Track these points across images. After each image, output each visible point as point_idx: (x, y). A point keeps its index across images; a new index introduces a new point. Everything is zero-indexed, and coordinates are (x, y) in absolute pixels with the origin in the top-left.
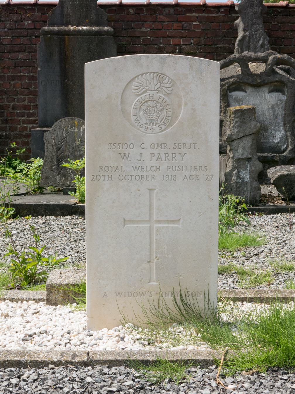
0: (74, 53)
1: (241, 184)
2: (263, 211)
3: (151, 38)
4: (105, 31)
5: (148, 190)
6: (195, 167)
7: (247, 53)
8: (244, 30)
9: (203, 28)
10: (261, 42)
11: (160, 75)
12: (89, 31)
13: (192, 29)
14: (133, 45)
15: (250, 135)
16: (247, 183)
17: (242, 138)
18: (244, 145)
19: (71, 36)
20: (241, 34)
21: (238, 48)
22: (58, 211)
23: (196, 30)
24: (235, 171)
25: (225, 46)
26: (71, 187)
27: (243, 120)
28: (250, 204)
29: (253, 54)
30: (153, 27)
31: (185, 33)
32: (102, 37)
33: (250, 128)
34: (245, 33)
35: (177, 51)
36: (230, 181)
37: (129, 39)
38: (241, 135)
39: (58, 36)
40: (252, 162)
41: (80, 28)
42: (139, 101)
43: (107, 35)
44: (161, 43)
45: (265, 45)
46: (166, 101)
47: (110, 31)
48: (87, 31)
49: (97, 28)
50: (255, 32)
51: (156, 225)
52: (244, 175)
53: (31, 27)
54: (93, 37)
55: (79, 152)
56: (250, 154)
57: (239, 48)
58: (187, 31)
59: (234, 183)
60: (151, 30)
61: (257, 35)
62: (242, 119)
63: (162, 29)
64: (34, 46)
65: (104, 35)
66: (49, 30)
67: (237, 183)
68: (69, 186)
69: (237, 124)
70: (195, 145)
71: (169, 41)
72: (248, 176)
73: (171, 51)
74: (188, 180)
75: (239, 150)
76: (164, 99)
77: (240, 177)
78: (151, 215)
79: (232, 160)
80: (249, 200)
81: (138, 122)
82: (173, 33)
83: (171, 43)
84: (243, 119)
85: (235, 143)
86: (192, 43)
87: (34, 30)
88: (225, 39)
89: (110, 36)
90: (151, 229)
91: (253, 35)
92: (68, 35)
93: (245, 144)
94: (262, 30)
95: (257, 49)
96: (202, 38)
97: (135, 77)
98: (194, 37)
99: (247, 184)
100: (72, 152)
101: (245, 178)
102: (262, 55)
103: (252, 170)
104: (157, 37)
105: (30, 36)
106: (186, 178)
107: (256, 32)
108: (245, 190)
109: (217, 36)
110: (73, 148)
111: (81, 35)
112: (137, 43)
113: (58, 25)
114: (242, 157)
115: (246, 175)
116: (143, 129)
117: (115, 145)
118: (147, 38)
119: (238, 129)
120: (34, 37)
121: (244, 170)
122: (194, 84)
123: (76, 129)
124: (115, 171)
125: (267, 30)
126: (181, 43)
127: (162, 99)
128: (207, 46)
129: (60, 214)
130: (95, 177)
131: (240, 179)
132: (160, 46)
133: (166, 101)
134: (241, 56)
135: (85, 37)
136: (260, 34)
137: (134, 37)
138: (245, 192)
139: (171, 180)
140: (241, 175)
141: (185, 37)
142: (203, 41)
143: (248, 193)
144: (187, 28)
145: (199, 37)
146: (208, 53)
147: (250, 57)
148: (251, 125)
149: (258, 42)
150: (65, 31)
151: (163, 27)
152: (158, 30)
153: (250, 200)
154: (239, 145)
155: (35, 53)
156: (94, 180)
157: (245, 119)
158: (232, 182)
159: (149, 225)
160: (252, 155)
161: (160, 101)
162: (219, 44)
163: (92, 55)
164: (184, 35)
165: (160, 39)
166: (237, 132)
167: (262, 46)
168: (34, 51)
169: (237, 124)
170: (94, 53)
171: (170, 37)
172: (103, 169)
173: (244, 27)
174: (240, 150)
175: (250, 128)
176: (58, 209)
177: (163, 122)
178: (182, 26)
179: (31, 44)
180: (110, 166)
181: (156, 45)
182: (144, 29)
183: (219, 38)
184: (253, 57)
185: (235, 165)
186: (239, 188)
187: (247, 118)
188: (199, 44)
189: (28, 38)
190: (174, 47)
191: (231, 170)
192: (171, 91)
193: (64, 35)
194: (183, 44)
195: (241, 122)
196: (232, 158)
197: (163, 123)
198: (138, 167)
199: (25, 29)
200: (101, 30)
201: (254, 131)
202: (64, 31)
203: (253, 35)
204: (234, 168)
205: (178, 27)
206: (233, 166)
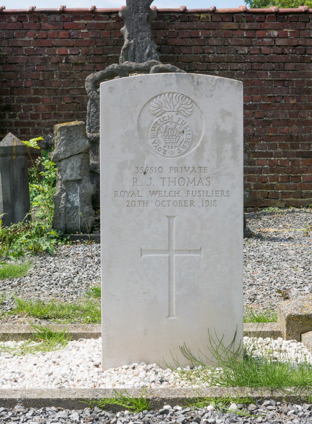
1: (71, 209)
2: (94, 239)
3: (34, 47)
5: (167, 218)
6: (217, 192)
7: (127, 63)
8: (129, 38)
9: (93, 36)
10: (147, 51)
11: (180, 96)
13: (80, 37)
15: (79, 154)
16: (77, 207)
17: (69, 158)
18: (72, 166)
20: (126, 42)
21: (122, 58)
23: (85, 39)
24: (63, 195)
25: (116, 55)
27: (69, 138)
28: (81, 231)
29: (133, 64)
30: (37, 35)
31: (72, 42)
33: (78, 146)
34: (130, 41)
35: (64, 61)
36: (59, 206)
38: (68, 154)
40: (82, 184)
42: (157, 123)
44: (45, 53)
45: (152, 54)
46: (185, 123)
50: (140, 40)
51: (175, 255)
52: (73, 199)
56: (80, 175)
57: (124, 58)
58: (74, 40)
59: (62, 208)
60: (34, 39)
61: (143, 43)
62: (68, 137)
63: (47, 38)
64: (238, 71)
67: (65, 207)
69: (63, 143)
71: (55, 51)
72: (78, 200)
73: (57, 62)
75: (67, 171)
76: (183, 121)
77: (69, 201)
78: (170, 245)
79: (60, 182)
80: (80, 226)
81: (156, 145)
82: (59, 43)
83: (57, 53)
84: (70, 136)
85: (63, 163)
86: (80, 53)
88: (117, 48)
91: (138, 43)
93: (73, 164)
94: (149, 38)
95: (144, 58)
96: (91, 47)
97: (153, 99)
98: (83, 46)
99: (77, 209)
101: (75, 202)
102: (144, 65)
103: (82, 193)
104: (42, 47)
107: (142, 39)
108: (75, 216)
109: (107, 45)
114: (70, 179)
115: (76, 199)
116: (161, 153)
117: (152, 169)
118: (30, 47)
119: (65, 148)
121: (73, 194)
122: (218, 104)
124: (131, 197)
125: (164, 37)
126: (67, 52)
127: (182, 120)
128: (96, 56)
130: (130, 203)
131: (70, 203)
132: (45, 57)
133: (185, 123)
134: (119, 66)
136: (146, 42)
138: (75, 217)
139: (211, 206)
140: (70, 199)
141: (73, 47)
142: (92, 50)
143: (78, 218)
144: (75, 37)
145: (88, 47)
146: (98, 63)
147: (130, 67)
148: (79, 143)
149: (144, 51)
151: (48, 36)
152: (41, 38)
153: (81, 227)
154: (67, 165)
156: (129, 206)
157: (72, 137)
158: (60, 207)
159: (167, 255)
160: (83, 176)
161: (180, 122)
162: (110, 54)
164: (71, 45)
165: (45, 49)
166: (64, 151)
167: (149, 55)
169: (63, 143)
171: (56, 46)
172: (119, 194)
173: (129, 35)
174: (68, 171)
175: (78, 146)
177: (183, 145)
178: (69, 34)
180: (126, 191)
181: (41, 55)
182: (27, 39)
183: (111, 47)
184: (133, 67)
185: (63, 187)
186: (68, 213)
187: (74, 136)
188: (88, 54)
190: (60, 57)
191: (59, 193)
192: (191, 112)
194: (70, 54)
195: (67, 140)
196: (61, 180)
197: (183, 146)
198: (155, 192)
201: (82, 150)
203: (138, 43)
204: (62, 191)
205: (64, 35)
206: (61, 188)
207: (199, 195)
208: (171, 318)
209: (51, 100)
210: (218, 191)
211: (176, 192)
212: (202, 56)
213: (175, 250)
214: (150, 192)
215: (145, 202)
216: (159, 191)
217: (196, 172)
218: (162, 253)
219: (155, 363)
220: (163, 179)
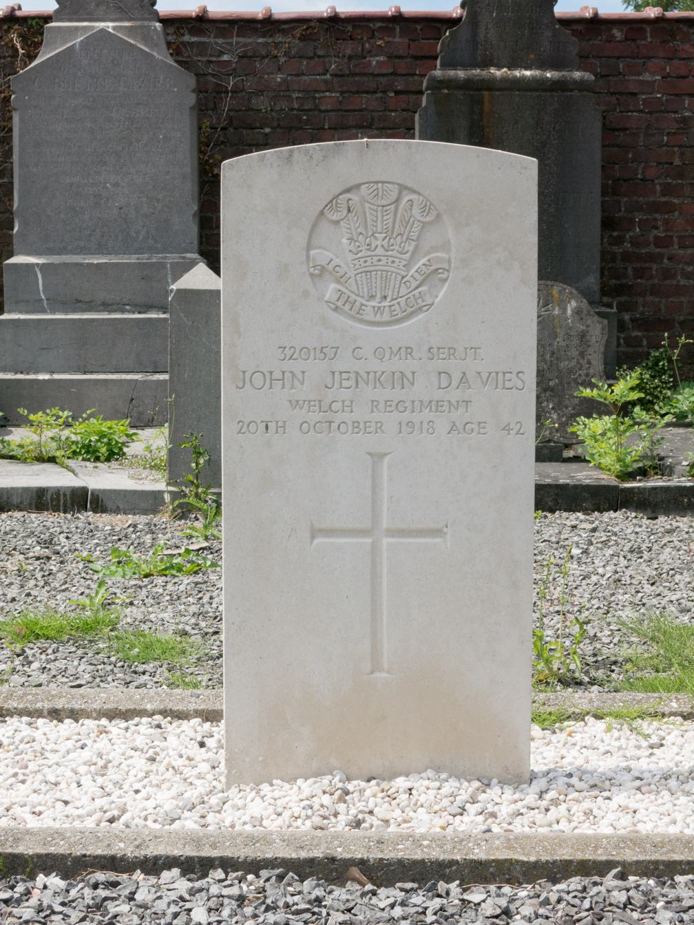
0: (504, 131)
4: (575, 82)
6: (440, 403)
12: (538, 81)
14: (621, 112)
19: (498, 93)
22: (585, 500)
26: (555, 442)
32: (569, 93)
37: (613, 99)
39: (467, 92)
41: (517, 73)
43: (580, 91)
47: (587, 81)
48: (534, 79)
49: (557, 73)
51: (386, 541)
53: (384, 71)
54: (549, 94)
55: (567, 362)
64: (393, 114)
65: (572, 90)
66: (446, 78)
68: (549, 441)
70: (475, 352)
74: (459, 433)
87: (392, 77)
89: (586, 93)
90: (375, 550)
92: (489, 89)
100: (551, 361)
105: (384, 92)
106: (454, 428)
110: (553, 353)
111: (518, 90)
112: (631, 108)
113: (465, 66)
120: (392, 94)
123: (557, 308)
129: (591, 507)
130: (245, 427)
135: (530, 93)
137: (623, 93)
150: (483, 81)
155: (395, 131)
159: (369, 540)
163: (545, 137)
168: (392, 126)
170: (549, 132)
176: (586, 495)
179: (385, 110)
189: (380, 95)
193: (479, 90)
198: (301, 402)
199: (372, 74)
200: (566, 78)
202: (480, 80)
207: (520, 375)
210: (511, 373)
211: (346, 404)
212: (377, 61)
214: (290, 401)
215: (280, 424)
216: (310, 401)
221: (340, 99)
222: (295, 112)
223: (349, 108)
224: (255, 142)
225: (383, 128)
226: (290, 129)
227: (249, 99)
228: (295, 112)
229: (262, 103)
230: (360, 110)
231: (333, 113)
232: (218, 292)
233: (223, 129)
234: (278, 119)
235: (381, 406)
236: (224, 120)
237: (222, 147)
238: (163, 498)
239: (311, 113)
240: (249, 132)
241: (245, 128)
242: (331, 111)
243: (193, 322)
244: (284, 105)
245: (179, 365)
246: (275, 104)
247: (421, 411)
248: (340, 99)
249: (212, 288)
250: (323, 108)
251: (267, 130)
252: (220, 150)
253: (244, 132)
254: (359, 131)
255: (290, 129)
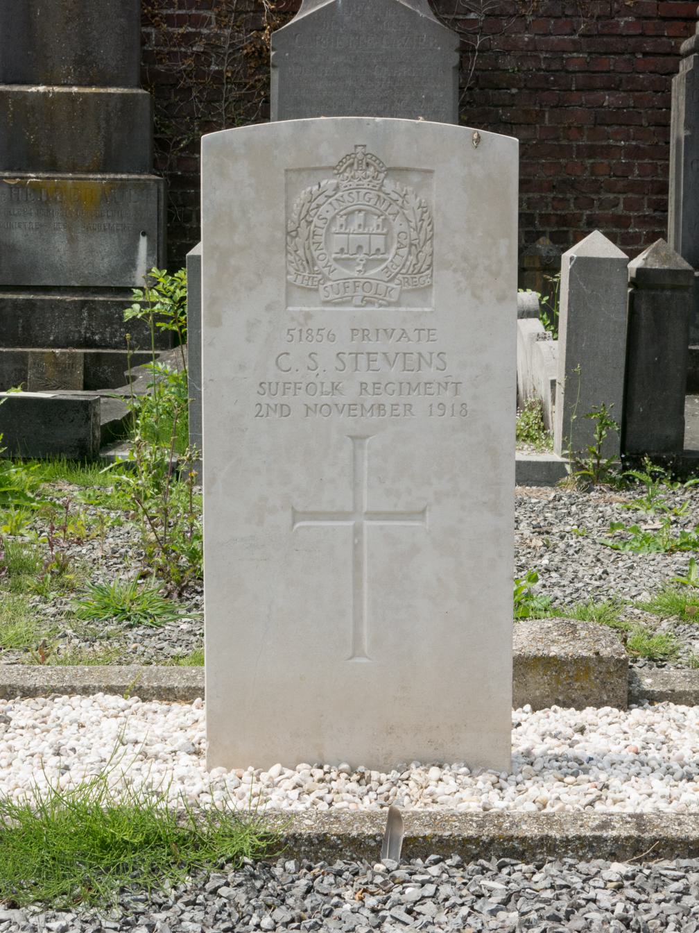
5: (349, 439)
168: (640, 88)
208: (357, 660)
209: (193, 172)
210: (290, 383)
213: (366, 513)
217: (409, 340)
218: (311, 519)
219: (300, 761)
220: (356, 357)
221: (588, 60)
222: (542, 73)
223: (597, 69)
224: (501, 103)
225: (631, 91)
226: (537, 89)
227: (497, 59)
228: (542, 73)
229: (509, 63)
230: (608, 72)
231: (580, 75)
232: (200, 256)
233: (470, 89)
234: (525, 80)
235: (370, 389)
236: (471, 80)
237: (468, 107)
238: (565, 469)
239: (557, 74)
240: (496, 92)
241: (492, 89)
242: (579, 72)
243: (592, 291)
244: (531, 65)
245: (577, 335)
246: (522, 64)
247: (409, 394)
248: (588, 60)
249: (612, 257)
250: (571, 69)
251: (514, 91)
252: (466, 110)
253: (491, 92)
254: (606, 93)
255: (537, 89)
